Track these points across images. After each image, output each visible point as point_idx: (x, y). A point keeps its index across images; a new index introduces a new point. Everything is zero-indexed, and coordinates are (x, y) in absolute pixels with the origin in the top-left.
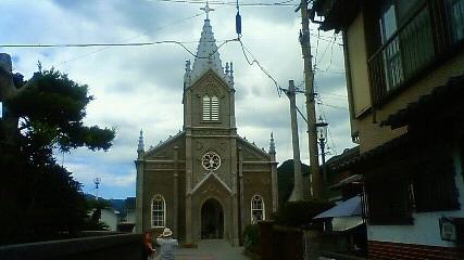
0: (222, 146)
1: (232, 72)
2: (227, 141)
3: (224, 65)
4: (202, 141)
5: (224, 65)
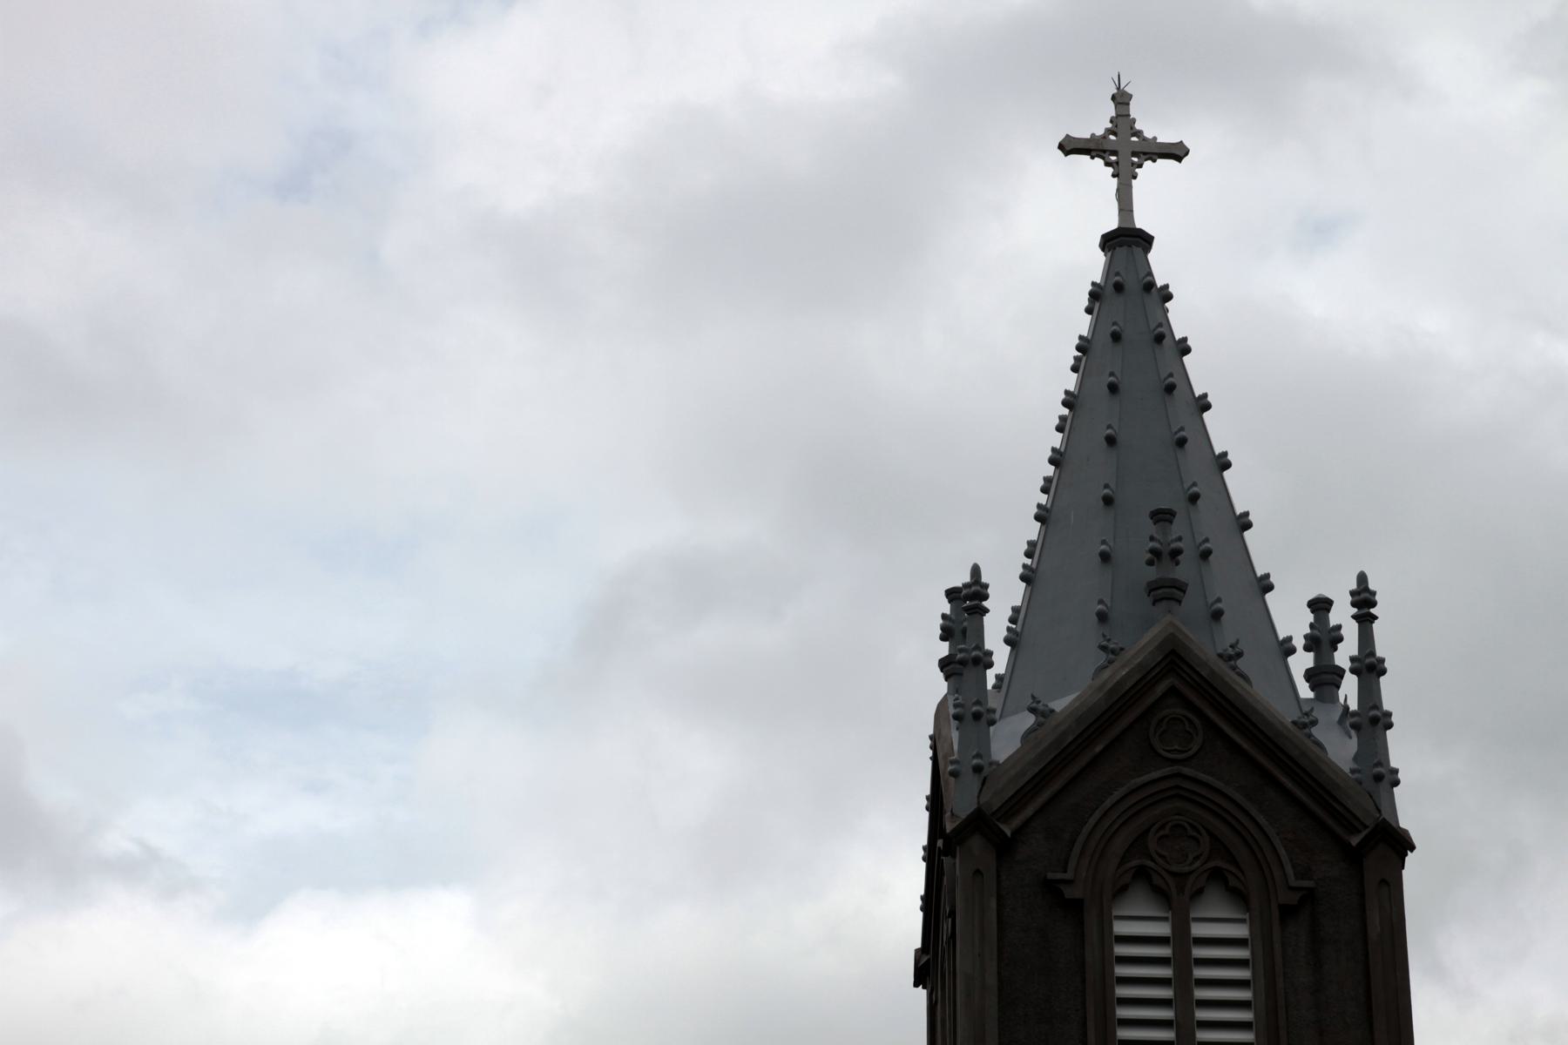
1: (1370, 668)
3: (1291, 620)
5: (1291, 620)
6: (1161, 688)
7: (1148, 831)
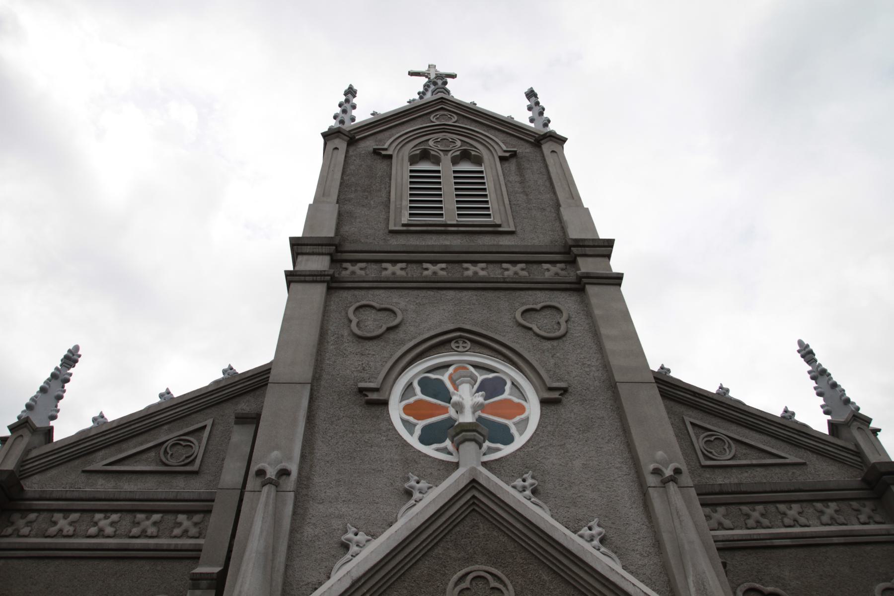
0: (541, 324)
2: (567, 303)
4: (397, 300)
6: (471, 502)
7: (430, 139)
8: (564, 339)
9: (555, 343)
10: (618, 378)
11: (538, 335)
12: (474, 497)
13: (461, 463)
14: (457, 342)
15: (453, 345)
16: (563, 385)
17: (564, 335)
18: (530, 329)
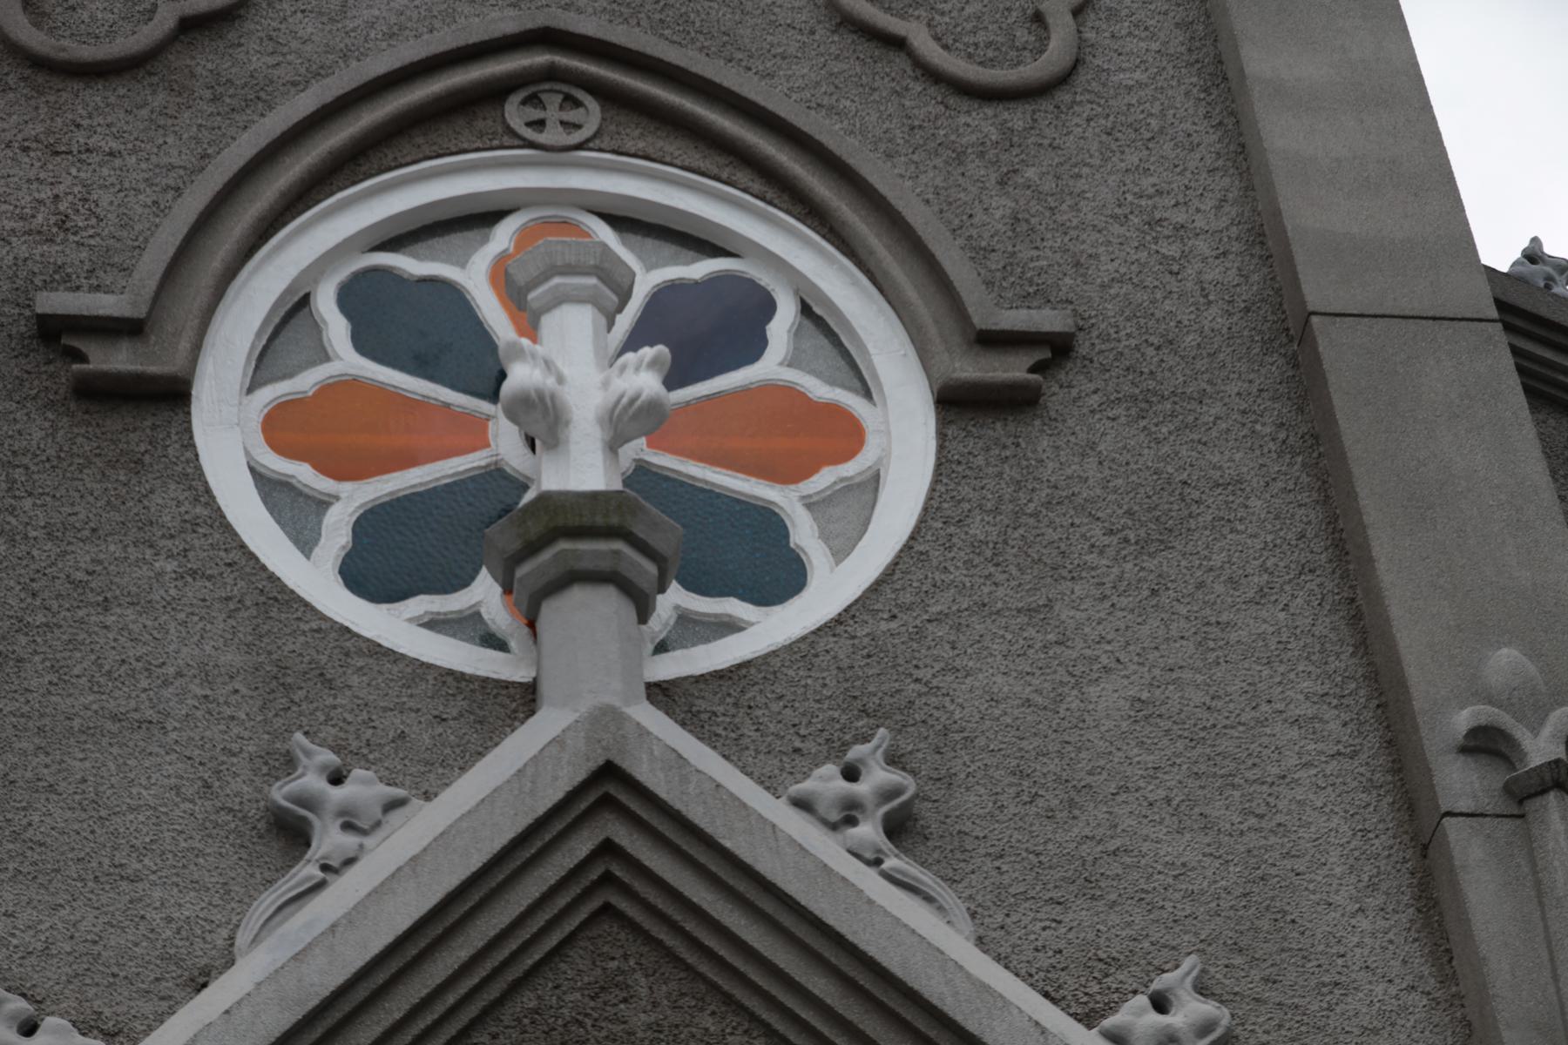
8: (1064, 96)
9: (1017, 117)
10: (1318, 291)
11: (934, 76)
12: (608, 848)
13: (545, 689)
14: (533, 100)
15: (515, 114)
16: (1049, 320)
17: (1063, 80)
18: (897, 43)
